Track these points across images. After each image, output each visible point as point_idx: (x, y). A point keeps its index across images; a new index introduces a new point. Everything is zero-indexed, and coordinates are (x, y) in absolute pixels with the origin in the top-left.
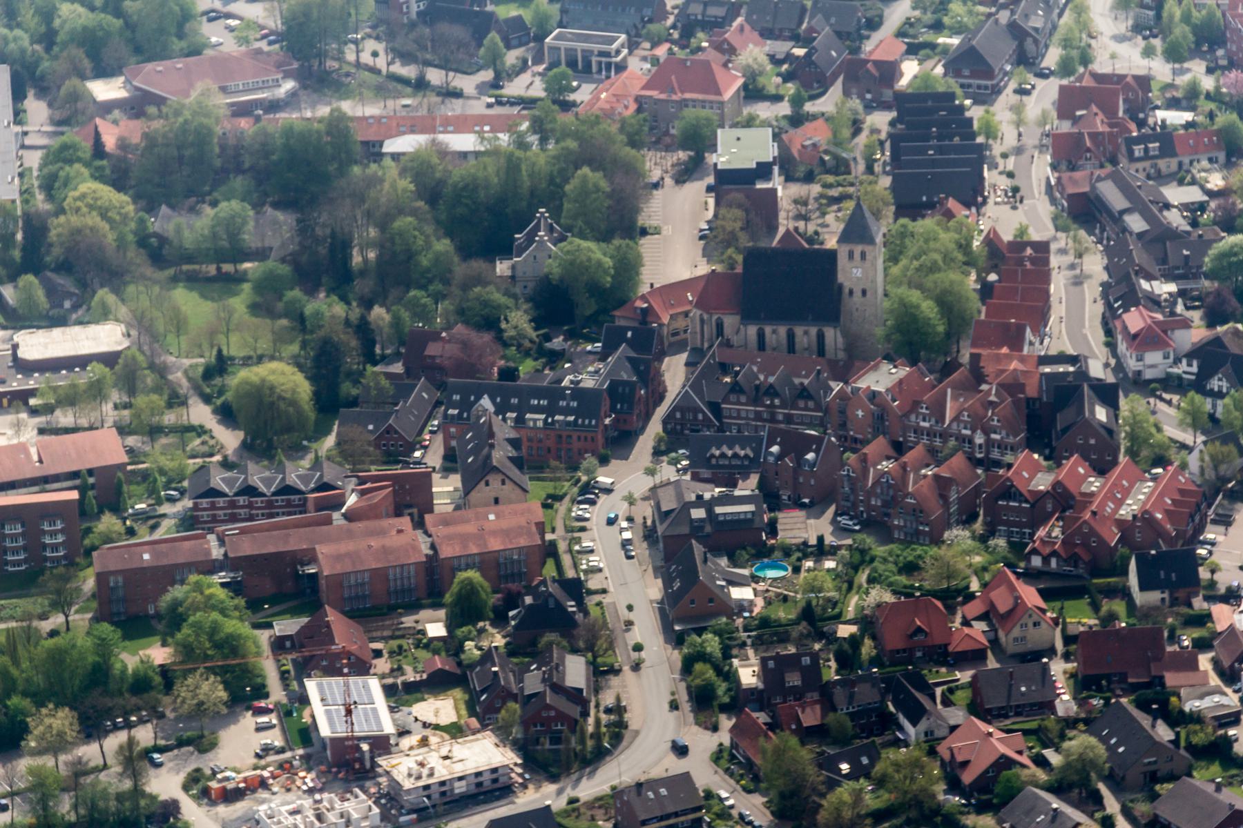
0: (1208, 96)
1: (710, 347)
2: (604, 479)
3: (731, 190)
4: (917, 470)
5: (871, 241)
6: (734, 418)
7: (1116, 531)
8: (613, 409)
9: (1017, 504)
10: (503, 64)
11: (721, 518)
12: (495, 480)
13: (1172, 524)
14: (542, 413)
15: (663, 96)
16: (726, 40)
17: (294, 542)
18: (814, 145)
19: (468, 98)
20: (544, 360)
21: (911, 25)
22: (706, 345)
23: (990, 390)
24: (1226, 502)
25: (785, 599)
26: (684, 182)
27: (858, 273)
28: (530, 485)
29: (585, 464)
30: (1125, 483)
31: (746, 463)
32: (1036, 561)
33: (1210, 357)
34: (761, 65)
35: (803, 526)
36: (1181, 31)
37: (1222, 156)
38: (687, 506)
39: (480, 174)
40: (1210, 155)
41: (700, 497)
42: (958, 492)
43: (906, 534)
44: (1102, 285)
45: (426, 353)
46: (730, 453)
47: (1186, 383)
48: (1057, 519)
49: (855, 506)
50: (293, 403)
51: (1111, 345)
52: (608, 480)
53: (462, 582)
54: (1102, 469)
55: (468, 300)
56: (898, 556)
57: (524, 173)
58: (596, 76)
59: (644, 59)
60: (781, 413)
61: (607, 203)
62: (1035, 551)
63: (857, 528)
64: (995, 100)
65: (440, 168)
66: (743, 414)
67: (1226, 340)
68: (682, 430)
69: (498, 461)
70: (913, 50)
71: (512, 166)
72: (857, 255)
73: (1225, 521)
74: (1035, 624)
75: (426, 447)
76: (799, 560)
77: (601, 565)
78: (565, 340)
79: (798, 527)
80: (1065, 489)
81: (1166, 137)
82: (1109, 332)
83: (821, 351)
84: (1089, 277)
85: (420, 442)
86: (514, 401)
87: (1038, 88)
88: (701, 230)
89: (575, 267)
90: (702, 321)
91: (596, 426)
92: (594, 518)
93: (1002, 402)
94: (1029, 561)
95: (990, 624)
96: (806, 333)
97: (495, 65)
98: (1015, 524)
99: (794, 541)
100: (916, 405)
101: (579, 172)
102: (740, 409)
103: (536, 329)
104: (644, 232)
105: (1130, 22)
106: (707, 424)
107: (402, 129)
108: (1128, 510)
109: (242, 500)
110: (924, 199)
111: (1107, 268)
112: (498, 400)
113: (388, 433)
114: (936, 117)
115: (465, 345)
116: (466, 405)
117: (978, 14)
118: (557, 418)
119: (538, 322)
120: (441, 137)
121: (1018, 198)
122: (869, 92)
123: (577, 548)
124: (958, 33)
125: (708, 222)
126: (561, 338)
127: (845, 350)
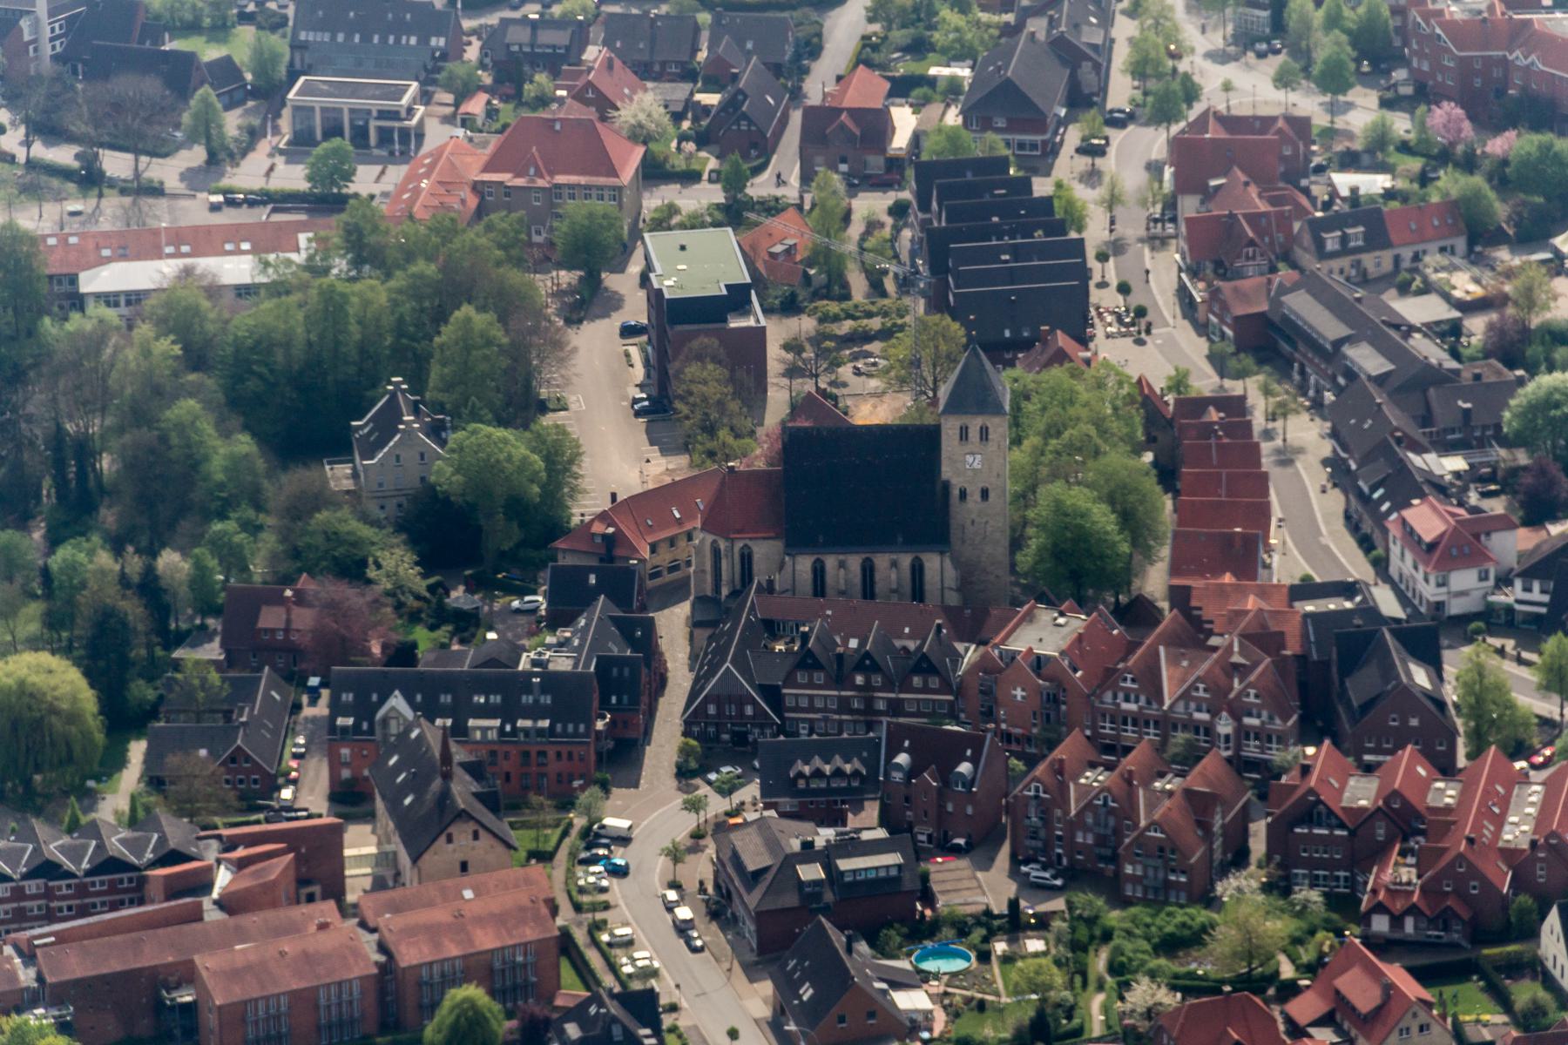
0: (1405, 148)
2: (612, 822)
4: (1147, 784)
6: (803, 710)
7: (1505, 868)
9: (1316, 831)
10: (222, 135)
11: (848, 879)
12: (462, 833)
14: (495, 717)
16: (590, 84)
17: (154, 953)
18: (789, 251)
19: (175, 196)
20: (450, 628)
21: (875, 48)
22: (725, 591)
23: (1231, 645)
25: (982, 1006)
26: (580, 321)
27: (975, 462)
29: (583, 798)
30: (1499, 788)
31: (855, 784)
32: (1380, 924)
35: (974, 884)
36: (1327, 46)
37: (1461, 243)
38: (790, 861)
41: (808, 845)
42: (1223, 818)
44: (1325, 462)
45: (261, 624)
47: (1518, 618)
48: (1403, 853)
49: (1047, 849)
50: (74, 717)
51: (1381, 566)
52: (624, 824)
53: (458, 1005)
54: (1446, 769)
56: (1148, 926)
58: (376, 152)
59: (448, 120)
60: (882, 699)
61: (504, 362)
62: (1379, 908)
63: (1058, 882)
66: (819, 704)
68: (718, 733)
70: (902, 88)
72: (974, 434)
74: (1421, 1029)
75: (295, 782)
76: (986, 940)
77: (656, 964)
79: (975, 886)
80: (1406, 804)
82: (1366, 544)
83: (918, 593)
86: (446, 699)
88: (635, 401)
90: (716, 553)
93: (1256, 665)
94: (1369, 924)
95: (1339, 1030)
96: (894, 564)
97: (209, 138)
98: (1321, 864)
99: (969, 910)
100: (1108, 678)
101: (457, 314)
102: (810, 696)
104: (543, 407)
105: (1230, 28)
107: (106, 253)
108: (1518, 830)
109: (32, 886)
110: (1007, 334)
111: (1334, 434)
112: (419, 698)
114: (987, 198)
115: (332, 607)
116: (364, 710)
117: (989, 26)
118: (520, 723)
119: (427, 564)
121: (1143, 327)
122: (844, 161)
123: (605, 938)
124: (958, 58)
125: (641, 386)
127: (958, 590)
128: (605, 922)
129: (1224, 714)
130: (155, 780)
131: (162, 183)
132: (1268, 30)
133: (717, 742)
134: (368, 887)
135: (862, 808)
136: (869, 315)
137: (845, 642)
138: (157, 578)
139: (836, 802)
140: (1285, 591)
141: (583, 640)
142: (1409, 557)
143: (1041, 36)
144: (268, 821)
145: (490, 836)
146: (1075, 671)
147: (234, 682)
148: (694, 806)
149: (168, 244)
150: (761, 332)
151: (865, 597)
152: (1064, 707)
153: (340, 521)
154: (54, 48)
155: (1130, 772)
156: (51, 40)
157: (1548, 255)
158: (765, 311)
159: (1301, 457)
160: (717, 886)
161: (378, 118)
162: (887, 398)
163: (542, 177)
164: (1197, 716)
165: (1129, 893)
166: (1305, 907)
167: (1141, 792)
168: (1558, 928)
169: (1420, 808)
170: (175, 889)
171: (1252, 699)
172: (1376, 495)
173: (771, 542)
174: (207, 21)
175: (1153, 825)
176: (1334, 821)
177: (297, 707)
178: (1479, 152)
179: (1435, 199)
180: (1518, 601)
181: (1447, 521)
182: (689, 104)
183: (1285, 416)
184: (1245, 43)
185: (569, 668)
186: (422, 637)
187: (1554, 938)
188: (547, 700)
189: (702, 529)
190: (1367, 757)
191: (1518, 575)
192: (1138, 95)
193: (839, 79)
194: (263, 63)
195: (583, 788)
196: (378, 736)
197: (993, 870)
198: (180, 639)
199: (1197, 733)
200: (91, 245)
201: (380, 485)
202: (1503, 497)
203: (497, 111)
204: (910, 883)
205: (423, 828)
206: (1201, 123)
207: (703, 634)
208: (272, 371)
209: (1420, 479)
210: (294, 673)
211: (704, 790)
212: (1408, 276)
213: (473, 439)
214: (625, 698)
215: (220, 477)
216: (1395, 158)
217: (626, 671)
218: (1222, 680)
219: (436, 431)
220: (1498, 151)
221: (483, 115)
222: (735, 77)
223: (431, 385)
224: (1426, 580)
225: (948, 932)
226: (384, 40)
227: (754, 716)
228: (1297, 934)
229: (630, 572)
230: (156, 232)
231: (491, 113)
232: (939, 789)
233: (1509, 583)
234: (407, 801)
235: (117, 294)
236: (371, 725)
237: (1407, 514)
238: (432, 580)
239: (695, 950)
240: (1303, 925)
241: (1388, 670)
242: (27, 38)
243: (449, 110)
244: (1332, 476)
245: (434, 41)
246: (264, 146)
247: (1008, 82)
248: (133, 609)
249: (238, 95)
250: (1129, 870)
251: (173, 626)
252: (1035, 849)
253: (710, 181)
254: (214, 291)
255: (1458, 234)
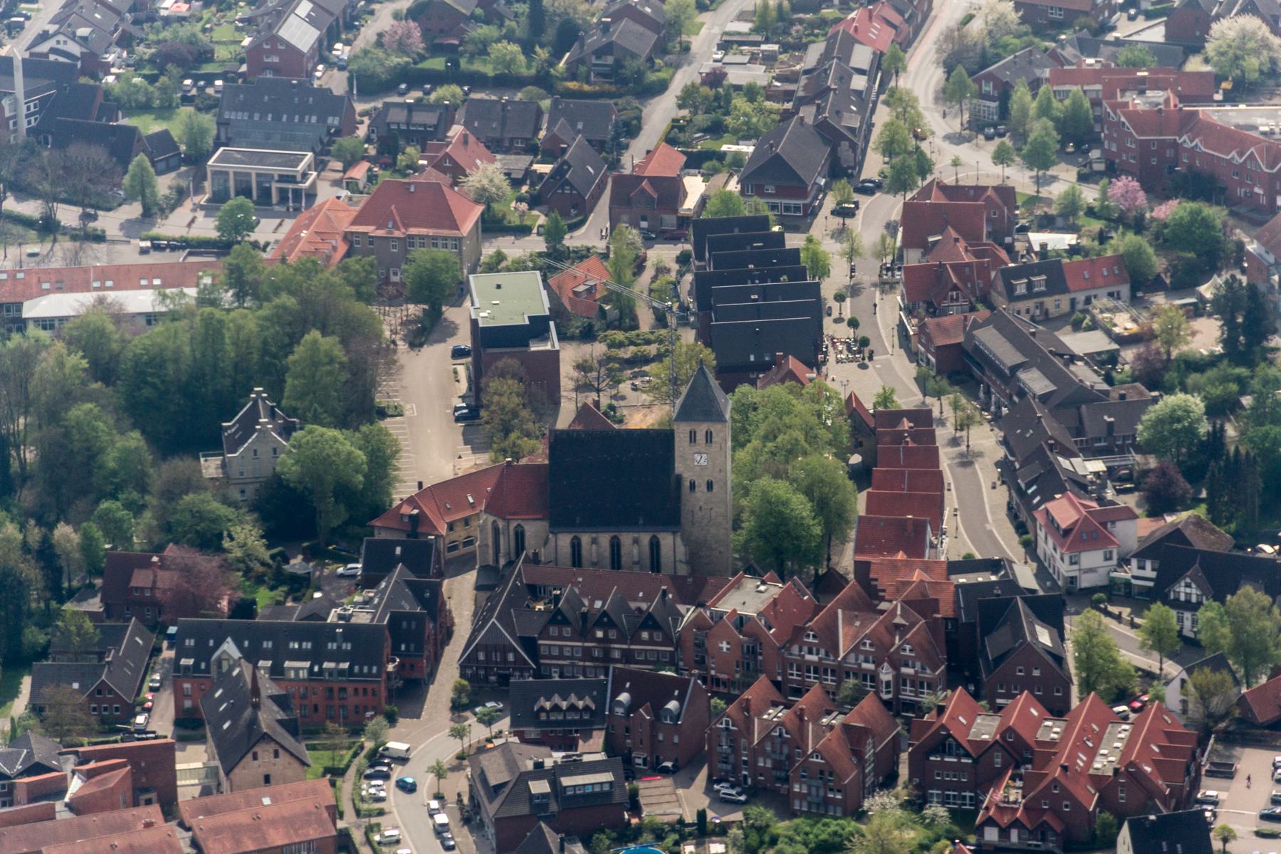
0: (1091, 212)
1: (511, 564)
3: (502, 354)
4: (816, 720)
5: (720, 418)
8: (395, 651)
10: (154, 194)
13: (1164, 780)
14: (306, 660)
15: (381, 233)
18: (590, 291)
19: (114, 242)
20: (285, 589)
21: (681, 129)
22: (502, 562)
23: (895, 608)
24: (1220, 747)
26: (421, 345)
27: (701, 460)
28: (309, 756)
29: (371, 725)
31: (586, 717)
33: (1169, 555)
34: (499, 188)
35: (673, 798)
36: (1039, 128)
37: (1125, 290)
38: (524, 778)
39: (171, 345)
40: (1111, 289)
41: (539, 765)
42: (874, 747)
43: (810, 804)
44: (998, 464)
45: (133, 584)
46: (564, 705)
47: (1135, 591)
48: (1013, 778)
49: (736, 770)
51: (1030, 547)
52: (402, 746)
54: (1058, 709)
55: (175, 512)
56: (807, 834)
57: (227, 341)
58: (277, 208)
59: (337, 183)
60: (617, 649)
61: (345, 376)
62: (990, 822)
63: (743, 798)
64: (811, 224)
65: (117, 336)
67: (1187, 533)
68: (486, 676)
69: (269, 727)
70: (695, 162)
71: (212, 332)
72: (701, 437)
73: (1225, 772)
75: (149, 710)
76: (677, 843)
78: (306, 560)
81: (1048, 263)
82: (1021, 528)
83: (656, 565)
84: (980, 454)
85: (142, 704)
86: (268, 645)
87: (863, 207)
88: (457, 409)
89: (318, 464)
90: (496, 531)
91: (379, 674)
92: (392, 798)
93: (913, 625)
94: (982, 835)
96: (636, 541)
97: (144, 196)
99: (666, 819)
100: (798, 633)
101: (306, 337)
103: (269, 547)
104: (382, 414)
105: (966, 117)
106: (521, 666)
107: (46, 286)
108: (1105, 762)
110: (752, 358)
111: (1005, 442)
112: (246, 643)
113: (99, 692)
114: (748, 249)
115: (187, 571)
116: (203, 653)
117: (771, 112)
118: (326, 665)
119: (271, 537)
120: (111, 296)
121: (867, 355)
122: (644, 219)
123: (377, 838)
124: (746, 138)
125: (463, 398)
126: (300, 557)
128: (378, 825)
129: (886, 664)
130: (36, 708)
131: (104, 231)
132: (995, 117)
133: (486, 682)
134: (197, 795)
135: (591, 737)
136: (648, 342)
137: (592, 603)
138: (51, 546)
139: (571, 731)
140: (944, 566)
141: (381, 599)
142: (1050, 541)
143: (809, 120)
144: (123, 741)
145: (287, 755)
146: (770, 628)
147: (104, 630)
148: (459, 734)
149: (95, 280)
150: (554, 356)
151: (613, 568)
152: (760, 658)
153: (203, 501)
154: (29, 122)
155: (802, 710)
156: (27, 116)
157: (1193, 300)
158: (560, 340)
159: (980, 459)
160: (472, 798)
161: (278, 181)
162: (655, 409)
163: (398, 229)
164: (865, 665)
165: (797, 807)
166: (933, 820)
167: (756, 721)
168: (1128, 840)
169: (1031, 742)
170: (36, 794)
171: (907, 653)
172: (1030, 491)
173: (539, 523)
174: (157, 103)
175: (816, 752)
176: (962, 752)
177: (157, 651)
178: (1148, 215)
179: (1109, 253)
180: (1134, 577)
181: (1078, 511)
182: (529, 173)
183: (968, 426)
184: (977, 126)
185: (367, 622)
186: (263, 597)
187: (1126, 847)
188: (347, 646)
189: (486, 511)
190: (999, 701)
191: (1134, 556)
192: (887, 169)
193: (648, 152)
194: (195, 135)
195: (372, 718)
196: (214, 674)
197: (692, 788)
198: (71, 594)
199: (865, 679)
200: (34, 281)
201: (242, 473)
202: (1136, 494)
203: (376, 176)
204: (618, 797)
205: (234, 750)
206: (926, 192)
207: (484, 595)
208: (163, 382)
209: (1064, 478)
210: (158, 623)
211: (472, 720)
212: (1081, 316)
213: (309, 438)
214: (412, 646)
215: (112, 465)
216: (1082, 220)
217: (414, 625)
218: (886, 638)
219: (287, 431)
220: (1162, 215)
221: (365, 180)
222: (564, 151)
223: (286, 394)
224: (1062, 559)
225: (647, 837)
226: (290, 119)
227: (515, 662)
228: (926, 842)
229: (428, 546)
230: (86, 271)
231: (371, 178)
232: (652, 724)
233: (1128, 562)
234: (226, 726)
235: (52, 319)
236: (208, 666)
237: (1050, 506)
238: (275, 551)
239: (451, 848)
240: (930, 834)
241: (1018, 632)
242: (7, 114)
243: (338, 175)
244: (1001, 474)
245: (330, 120)
246: (188, 204)
247: (778, 157)
248: (31, 571)
249: (173, 162)
250: (797, 788)
251: (66, 585)
252: (727, 772)
253: (539, 234)
254: (120, 318)
255: (1123, 282)
